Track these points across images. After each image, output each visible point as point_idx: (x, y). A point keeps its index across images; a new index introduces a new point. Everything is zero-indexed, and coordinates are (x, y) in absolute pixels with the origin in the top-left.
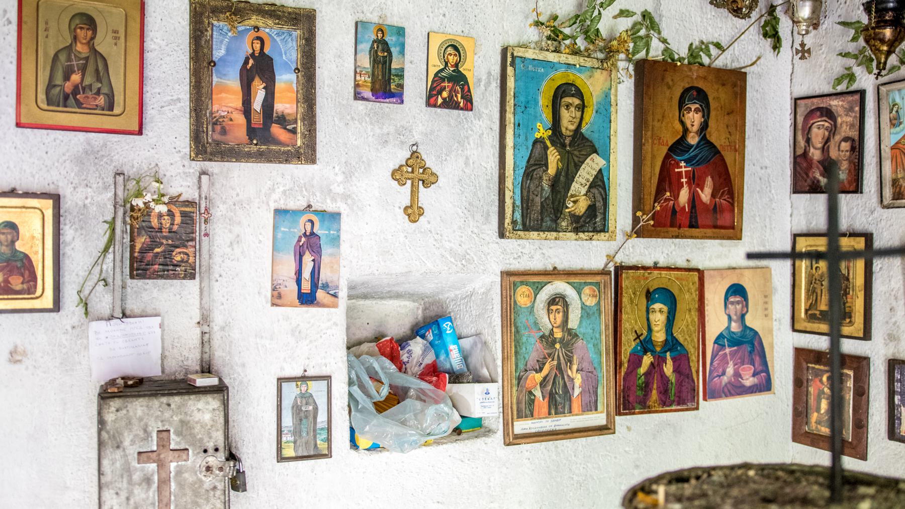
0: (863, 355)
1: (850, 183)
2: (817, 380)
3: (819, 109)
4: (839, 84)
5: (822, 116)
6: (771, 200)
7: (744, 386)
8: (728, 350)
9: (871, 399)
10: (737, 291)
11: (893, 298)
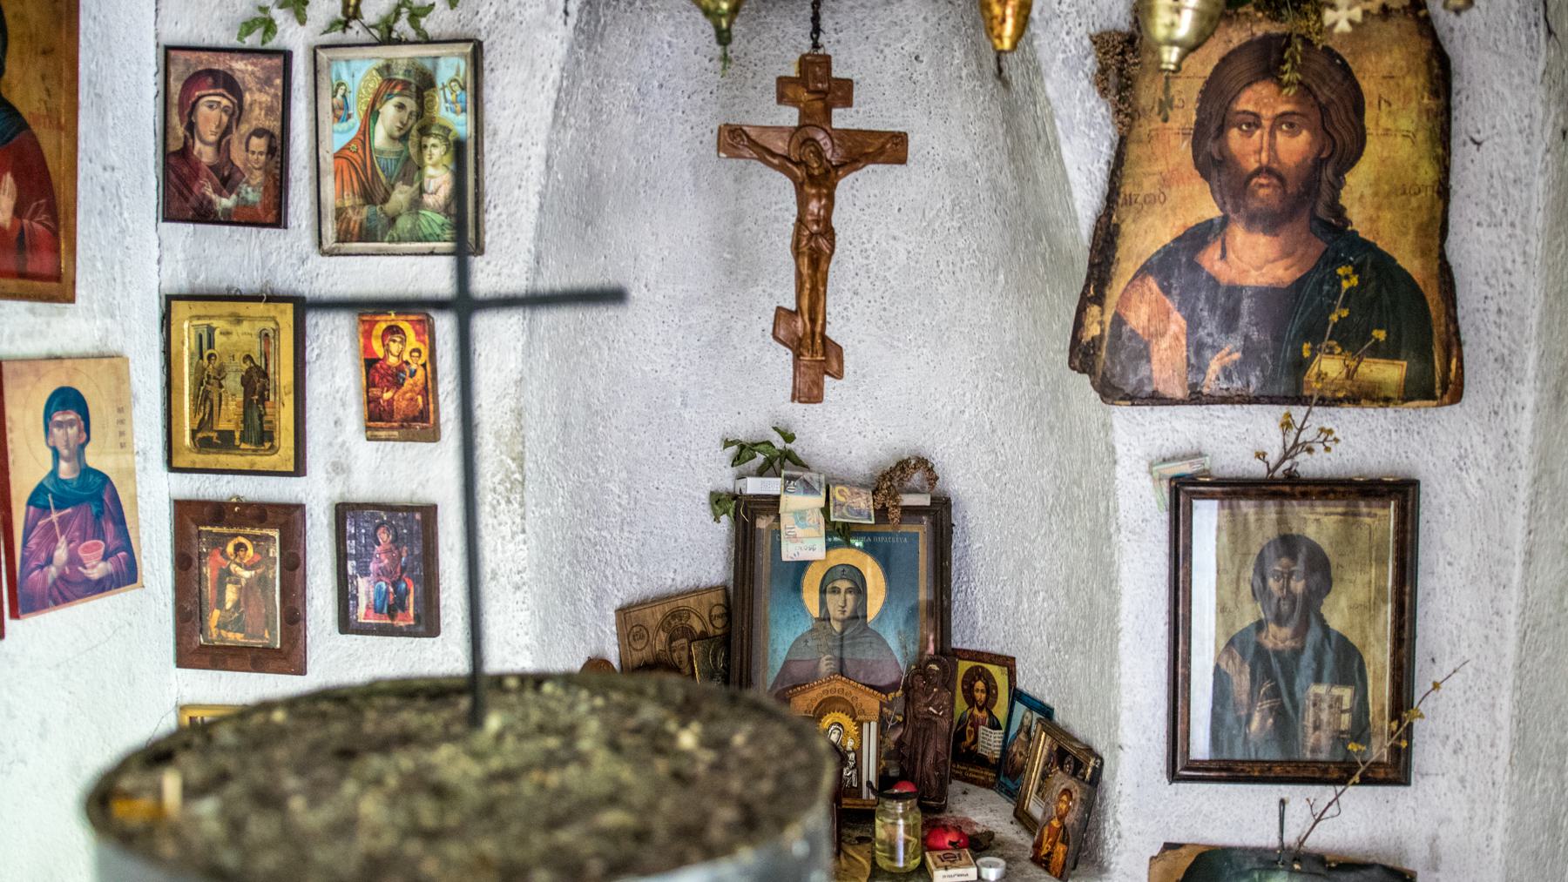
0: (293, 501)
1: (266, 209)
2: (216, 552)
3: (210, 72)
4: (248, 33)
5: (215, 86)
6: (122, 231)
7: (88, 580)
8: (54, 516)
9: (309, 573)
10: (68, 401)
11: (338, 403)
